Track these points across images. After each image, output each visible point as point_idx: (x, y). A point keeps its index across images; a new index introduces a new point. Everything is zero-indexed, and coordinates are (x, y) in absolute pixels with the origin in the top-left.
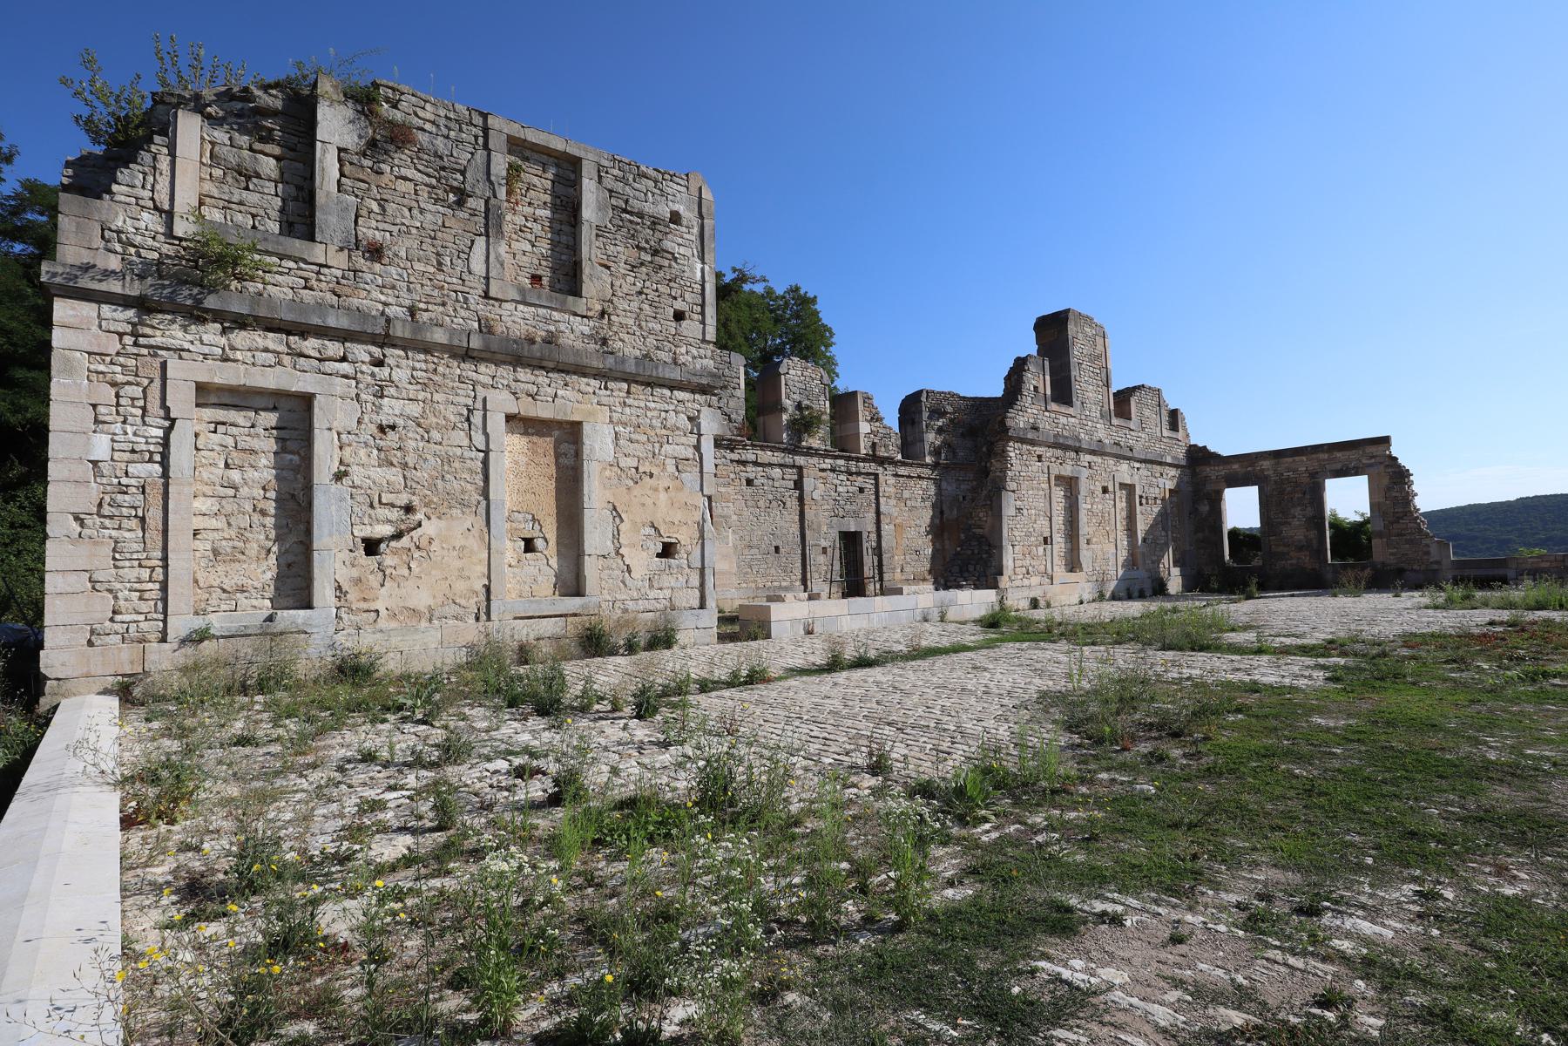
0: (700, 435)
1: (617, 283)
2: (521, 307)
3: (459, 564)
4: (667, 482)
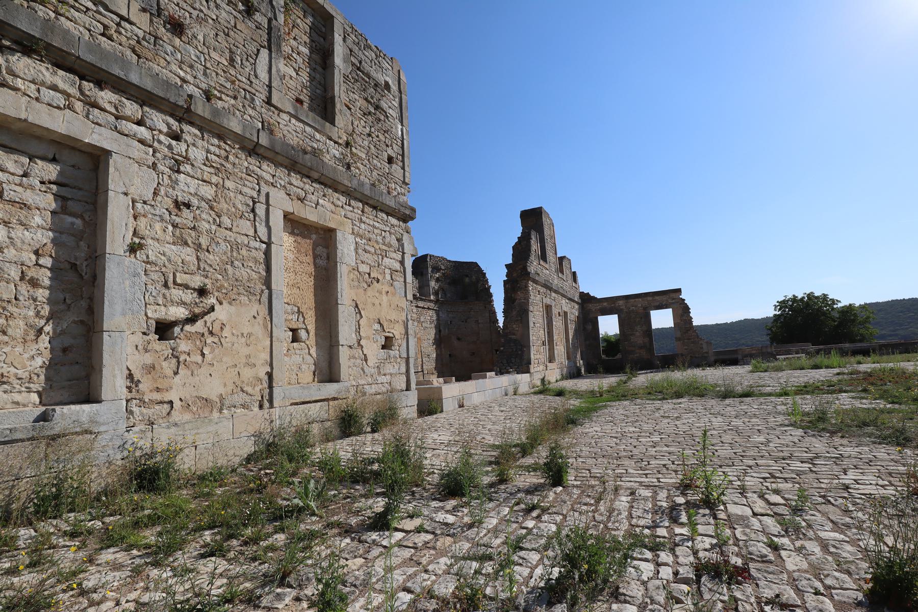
0: (404, 253)
1: (356, 123)
2: (293, 121)
3: (245, 351)
4: (386, 288)
